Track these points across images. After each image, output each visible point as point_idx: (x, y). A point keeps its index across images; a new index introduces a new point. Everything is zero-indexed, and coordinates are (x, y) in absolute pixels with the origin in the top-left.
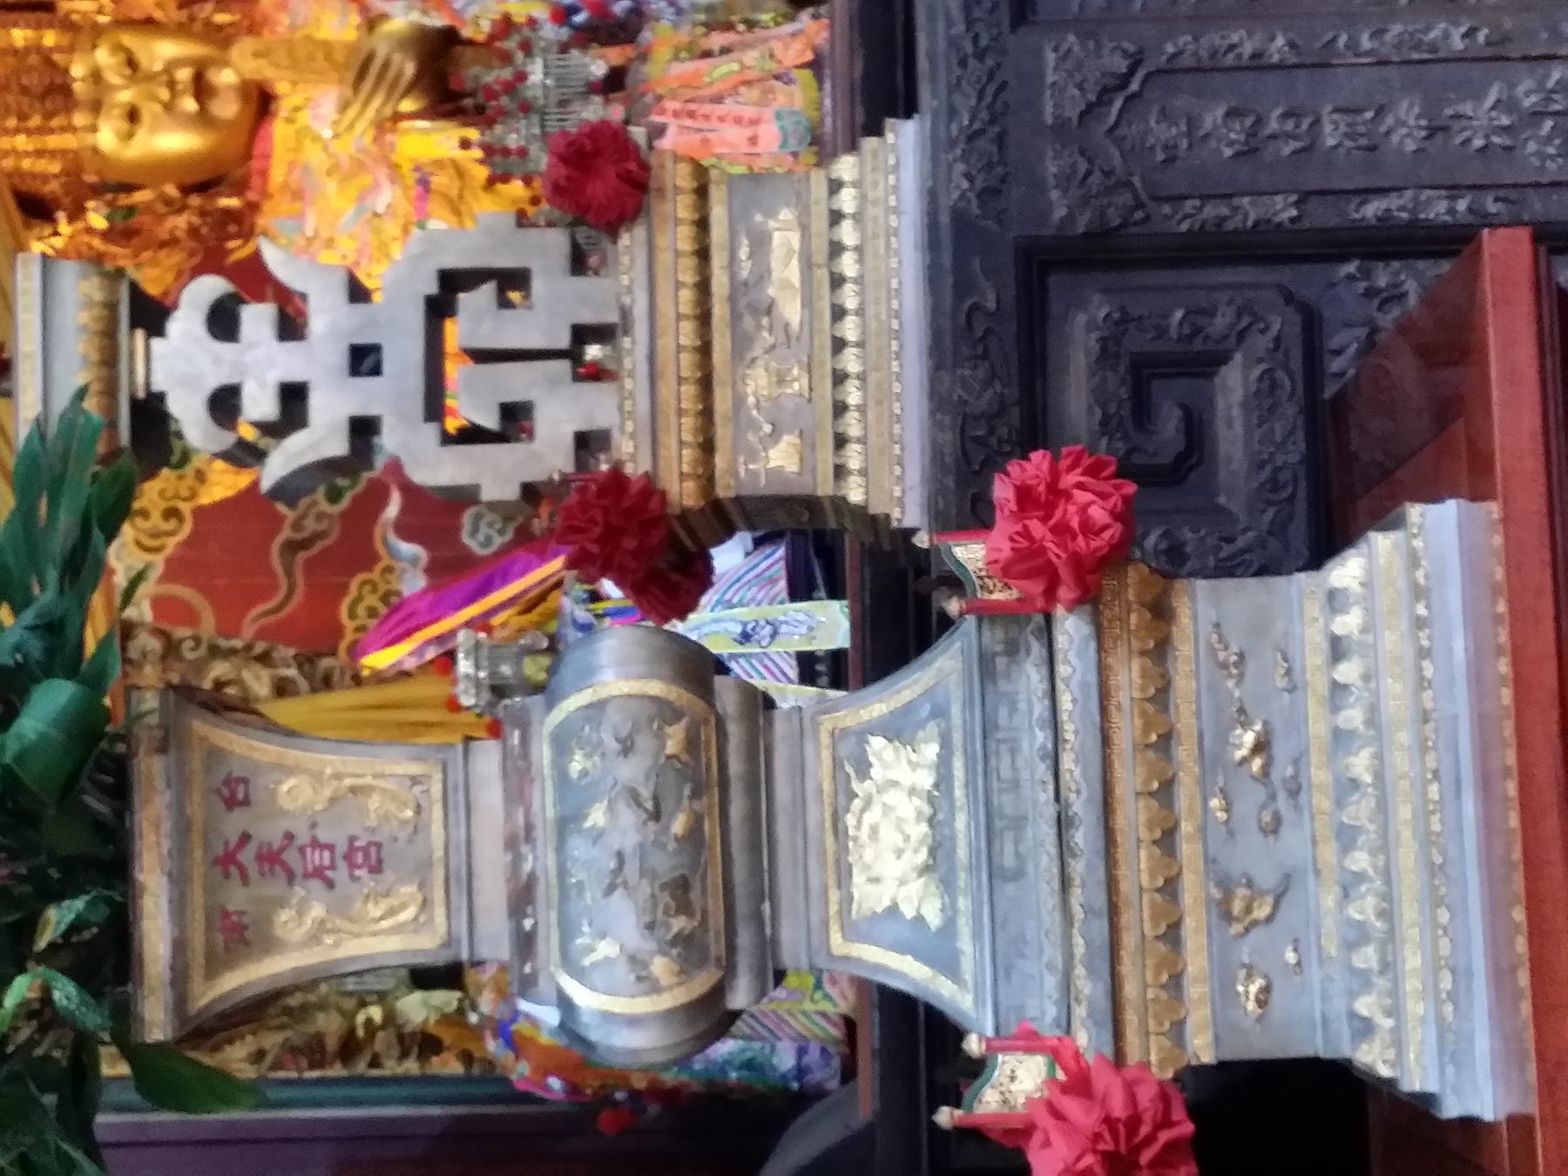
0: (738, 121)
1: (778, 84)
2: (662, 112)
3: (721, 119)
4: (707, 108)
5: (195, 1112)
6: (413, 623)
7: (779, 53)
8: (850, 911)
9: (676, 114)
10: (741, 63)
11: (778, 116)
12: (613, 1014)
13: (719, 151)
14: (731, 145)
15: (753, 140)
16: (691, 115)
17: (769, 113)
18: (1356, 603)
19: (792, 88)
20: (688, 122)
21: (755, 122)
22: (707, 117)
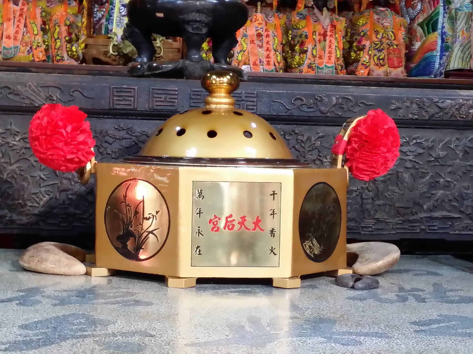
0: (17, 32)
1: (29, 48)
2: (23, 5)
3: (18, 26)
4: (23, 21)
5: (112, 48)
6: (357, 237)
7: (39, 49)
8: (55, 135)
9: (22, 10)
10: (37, 35)
11: (16, 47)
12: (289, 160)
13: (5, 24)
14: (7, 29)
15: (8, 37)
16: (21, 15)
17: (18, 44)
18: (376, 112)
19: (26, 53)
20: (18, 14)
21: (15, 39)
22: (19, 21)
